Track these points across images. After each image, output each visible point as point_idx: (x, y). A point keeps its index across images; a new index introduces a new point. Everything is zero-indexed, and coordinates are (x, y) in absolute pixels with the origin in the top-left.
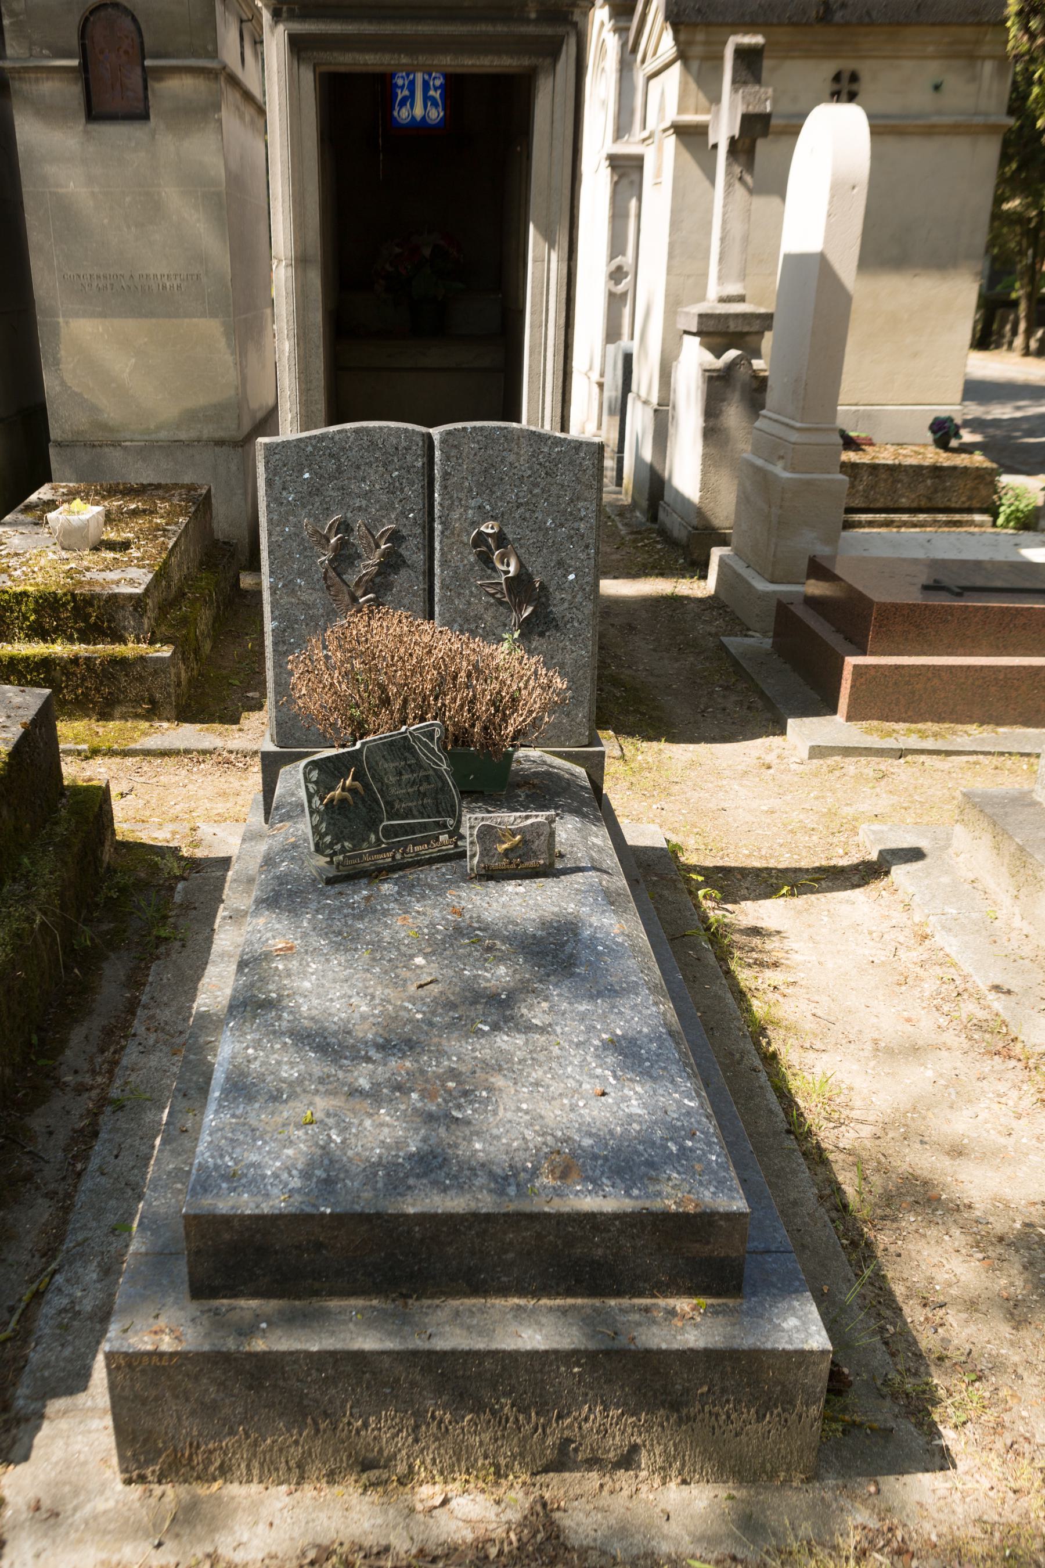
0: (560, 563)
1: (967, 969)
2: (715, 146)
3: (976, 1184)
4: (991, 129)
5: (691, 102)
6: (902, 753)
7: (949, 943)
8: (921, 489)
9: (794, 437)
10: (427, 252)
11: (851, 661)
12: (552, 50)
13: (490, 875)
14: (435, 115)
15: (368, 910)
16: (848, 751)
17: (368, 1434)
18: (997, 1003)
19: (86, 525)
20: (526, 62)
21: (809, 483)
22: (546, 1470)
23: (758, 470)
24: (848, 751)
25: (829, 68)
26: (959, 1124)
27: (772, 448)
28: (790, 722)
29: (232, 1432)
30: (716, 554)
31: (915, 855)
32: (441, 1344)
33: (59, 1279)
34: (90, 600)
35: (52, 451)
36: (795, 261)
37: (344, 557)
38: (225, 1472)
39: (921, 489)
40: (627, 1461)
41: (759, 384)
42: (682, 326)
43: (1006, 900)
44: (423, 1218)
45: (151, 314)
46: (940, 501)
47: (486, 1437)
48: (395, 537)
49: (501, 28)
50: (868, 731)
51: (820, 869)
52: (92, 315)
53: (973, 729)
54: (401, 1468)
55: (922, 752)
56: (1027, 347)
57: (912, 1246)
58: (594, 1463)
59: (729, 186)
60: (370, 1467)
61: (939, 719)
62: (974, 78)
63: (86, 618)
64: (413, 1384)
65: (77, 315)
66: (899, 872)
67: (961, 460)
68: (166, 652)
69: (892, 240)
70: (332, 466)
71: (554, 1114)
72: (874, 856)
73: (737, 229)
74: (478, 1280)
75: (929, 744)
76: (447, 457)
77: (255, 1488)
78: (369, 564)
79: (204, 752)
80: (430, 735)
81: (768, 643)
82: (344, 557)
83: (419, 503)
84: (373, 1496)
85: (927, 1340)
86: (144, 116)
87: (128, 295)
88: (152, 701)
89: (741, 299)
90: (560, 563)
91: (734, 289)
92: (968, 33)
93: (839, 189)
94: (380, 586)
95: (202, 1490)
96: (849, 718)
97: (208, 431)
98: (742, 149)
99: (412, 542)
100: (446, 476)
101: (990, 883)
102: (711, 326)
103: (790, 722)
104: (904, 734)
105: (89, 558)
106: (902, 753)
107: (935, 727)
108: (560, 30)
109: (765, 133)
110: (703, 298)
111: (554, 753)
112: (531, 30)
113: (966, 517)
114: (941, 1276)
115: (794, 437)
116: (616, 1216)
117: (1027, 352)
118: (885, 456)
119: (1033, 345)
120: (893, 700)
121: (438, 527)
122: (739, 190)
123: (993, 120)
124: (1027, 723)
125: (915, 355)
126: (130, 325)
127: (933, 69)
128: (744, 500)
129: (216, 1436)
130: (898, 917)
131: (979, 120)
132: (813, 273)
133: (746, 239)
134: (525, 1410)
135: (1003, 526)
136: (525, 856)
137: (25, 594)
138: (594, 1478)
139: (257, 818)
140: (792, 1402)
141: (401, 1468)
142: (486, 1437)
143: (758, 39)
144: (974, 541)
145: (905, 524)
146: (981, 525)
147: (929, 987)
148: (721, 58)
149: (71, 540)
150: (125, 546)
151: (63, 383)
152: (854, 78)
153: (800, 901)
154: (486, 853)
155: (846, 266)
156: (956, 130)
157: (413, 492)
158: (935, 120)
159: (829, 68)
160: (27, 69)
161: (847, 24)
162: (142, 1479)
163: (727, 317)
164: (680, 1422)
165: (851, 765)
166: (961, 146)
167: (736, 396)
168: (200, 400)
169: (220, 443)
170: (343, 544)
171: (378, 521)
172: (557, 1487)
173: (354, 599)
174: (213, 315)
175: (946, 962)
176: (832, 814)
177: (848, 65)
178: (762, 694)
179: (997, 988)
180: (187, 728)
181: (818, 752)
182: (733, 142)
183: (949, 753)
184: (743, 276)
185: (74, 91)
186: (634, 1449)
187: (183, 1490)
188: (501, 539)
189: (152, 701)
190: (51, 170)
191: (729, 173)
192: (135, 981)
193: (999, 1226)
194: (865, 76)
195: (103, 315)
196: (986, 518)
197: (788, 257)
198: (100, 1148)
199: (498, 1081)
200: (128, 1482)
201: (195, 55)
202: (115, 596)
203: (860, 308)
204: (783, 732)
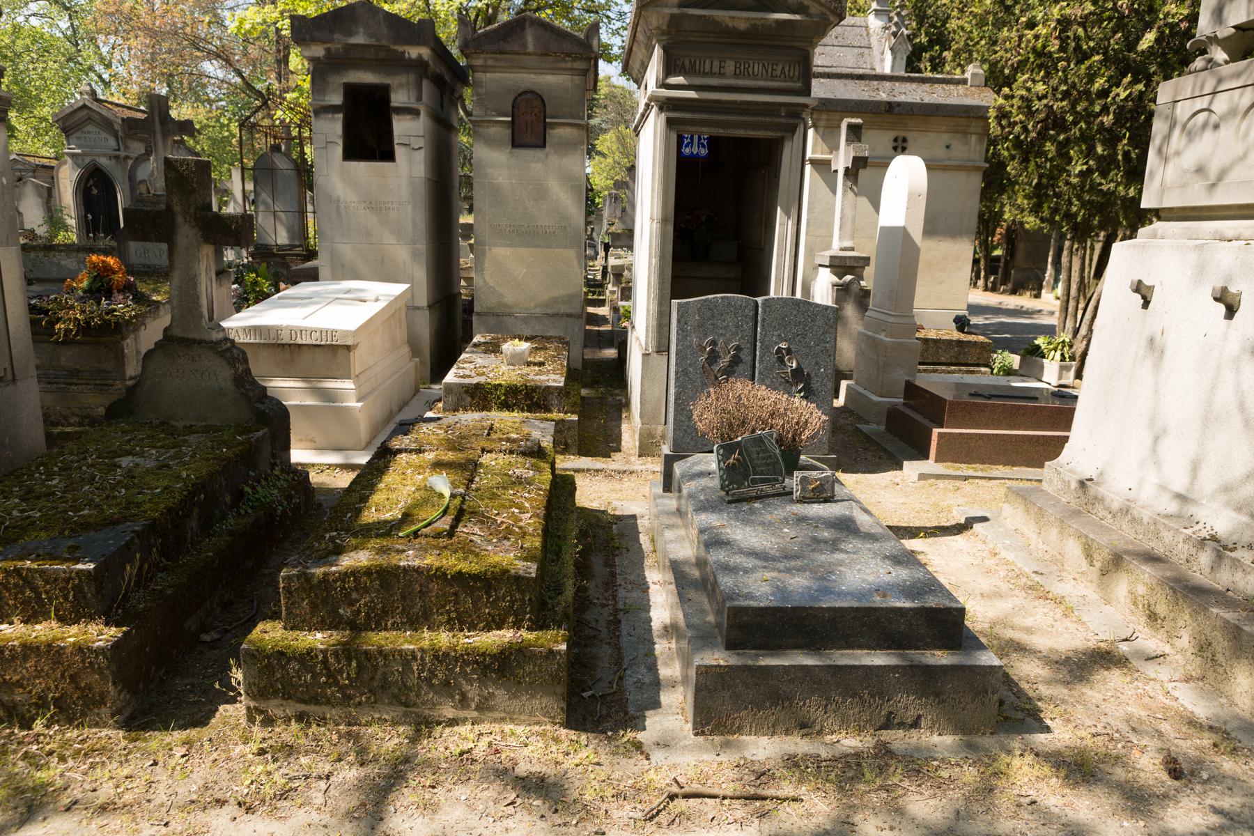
0: (817, 363)
1: (1019, 565)
2: (836, 171)
3: (1040, 642)
4: (976, 169)
5: (819, 148)
6: (966, 478)
7: (1010, 556)
8: (952, 353)
9: (891, 320)
10: (703, 218)
11: (936, 431)
12: (792, 130)
13: (803, 500)
14: (704, 152)
15: (752, 511)
16: (938, 477)
17: (805, 709)
18: (1037, 578)
19: (523, 352)
20: (779, 134)
21: (900, 344)
22: (880, 728)
23: (869, 337)
24: (938, 477)
25: (891, 135)
26: (1029, 622)
27: (880, 326)
28: (905, 463)
29: (746, 708)
30: (844, 384)
31: (984, 519)
32: (839, 663)
33: (628, 672)
34: (535, 389)
35: (474, 318)
36: (888, 232)
37: (713, 357)
38: (740, 730)
39: (952, 353)
40: (915, 724)
41: (866, 293)
42: (819, 261)
43: (1034, 537)
44: (829, 609)
45: (538, 246)
46: (962, 359)
47: (856, 710)
48: (738, 348)
49: (768, 119)
50: (947, 467)
51: (935, 528)
52: (505, 246)
53: (1000, 467)
54: (818, 727)
55: (977, 477)
56: (986, 286)
57: (1017, 664)
58: (901, 725)
59: (845, 191)
60: (805, 727)
61: (983, 463)
62: (967, 143)
63: (531, 399)
64: (827, 682)
65: (496, 245)
66: (977, 527)
67: (972, 338)
68: (575, 418)
69: (937, 223)
70: (709, 314)
71: (871, 578)
72: (963, 521)
73: (849, 213)
74: (849, 642)
75: (979, 474)
76: (764, 311)
77: (753, 737)
78: (724, 362)
79: (597, 471)
80: (771, 436)
81: (883, 428)
82: (713, 357)
83: (750, 333)
84: (806, 740)
85: (1031, 694)
86: (543, 146)
87: (527, 236)
88: (566, 444)
89: (852, 249)
90: (817, 363)
91: (848, 244)
92: (963, 121)
93: (912, 196)
94: (729, 371)
95: (730, 738)
96: (936, 461)
97: (563, 309)
98: (852, 174)
99: (746, 352)
100: (764, 320)
101: (1025, 530)
102: (837, 262)
103: (905, 463)
104: (965, 469)
105: (526, 370)
106: (966, 478)
107: (981, 466)
108: (797, 121)
109: (865, 166)
110: (829, 247)
111: (818, 460)
112: (783, 120)
113: (976, 369)
114: (1032, 674)
115: (891, 320)
116: (911, 609)
117: (986, 289)
118: (932, 335)
119: (990, 285)
120: (956, 451)
121: (758, 344)
122: (850, 193)
123: (977, 164)
124: (1028, 466)
125: (941, 283)
126: (525, 251)
127: (945, 138)
128: (860, 353)
129: (739, 711)
130: (980, 546)
131: (970, 164)
132: (897, 239)
133: (854, 219)
134: (873, 696)
135: (998, 374)
136: (821, 492)
137: (500, 385)
138: (901, 733)
139: (659, 489)
140: (986, 692)
141: (818, 727)
142: (856, 710)
143: (859, 121)
144: (982, 378)
145: (943, 371)
146: (985, 373)
147: (1002, 574)
148: (839, 127)
149: (515, 360)
150: (541, 364)
151: (485, 281)
152: (905, 140)
153: (931, 540)
154: (803, 489)
155: (916, 233)
156: (959, 168)
157: (748, 327)
158: (948, 163)
159: (891, 135)
160: (483, 121)
161: (900, 114)
162: (703, 733)
163: (845, 258)
164: (939, 703)
165: (941, 484)
166: (961, 176)
167: (852, 300)
168: (561, 292)
169: (569, 315)
170: (712, 351)
171: (730, 341)
172: (887, 735)
173: (717, 378)
174: (571, 247)
175: (1007, 563)
176: (935, 505)
177: (901, 134)
178: (886, 451)
179: (1036, 572)
180: (584, 459)
181: (923, 477)
182: (847, 169)
183: (990, 479)
184: (852, 237)
185: (507, 132)
186: (919, 717)
187: (722, 738)
188: (789, 351)
189: (566, 444)
190: (490, 171)
191: (844, 185)
192: (610, 564)
193: (1054, 657)
194: (910, 139)
195: (511, 246)
196: (987, 369)
197: (882, 228)
198: (625, 628)
199: (842, 569)
200: (696, 734)
201: (573, 117)
202: (548, 387)
203: (923, 256)
204: (901, 468)
